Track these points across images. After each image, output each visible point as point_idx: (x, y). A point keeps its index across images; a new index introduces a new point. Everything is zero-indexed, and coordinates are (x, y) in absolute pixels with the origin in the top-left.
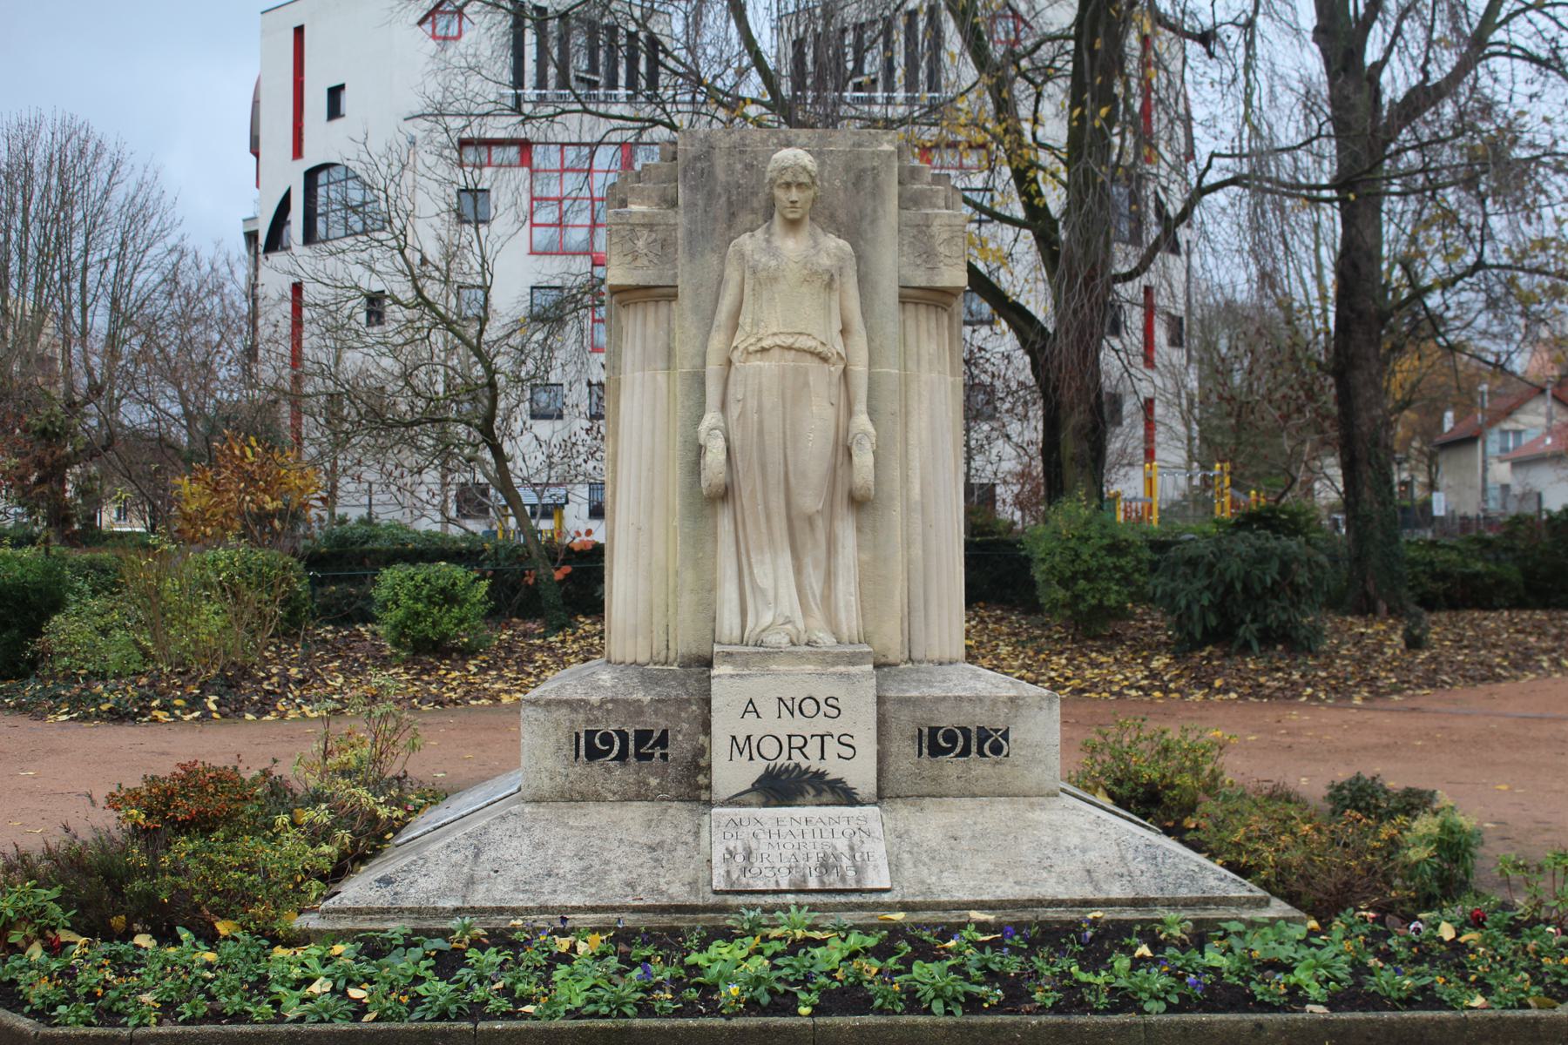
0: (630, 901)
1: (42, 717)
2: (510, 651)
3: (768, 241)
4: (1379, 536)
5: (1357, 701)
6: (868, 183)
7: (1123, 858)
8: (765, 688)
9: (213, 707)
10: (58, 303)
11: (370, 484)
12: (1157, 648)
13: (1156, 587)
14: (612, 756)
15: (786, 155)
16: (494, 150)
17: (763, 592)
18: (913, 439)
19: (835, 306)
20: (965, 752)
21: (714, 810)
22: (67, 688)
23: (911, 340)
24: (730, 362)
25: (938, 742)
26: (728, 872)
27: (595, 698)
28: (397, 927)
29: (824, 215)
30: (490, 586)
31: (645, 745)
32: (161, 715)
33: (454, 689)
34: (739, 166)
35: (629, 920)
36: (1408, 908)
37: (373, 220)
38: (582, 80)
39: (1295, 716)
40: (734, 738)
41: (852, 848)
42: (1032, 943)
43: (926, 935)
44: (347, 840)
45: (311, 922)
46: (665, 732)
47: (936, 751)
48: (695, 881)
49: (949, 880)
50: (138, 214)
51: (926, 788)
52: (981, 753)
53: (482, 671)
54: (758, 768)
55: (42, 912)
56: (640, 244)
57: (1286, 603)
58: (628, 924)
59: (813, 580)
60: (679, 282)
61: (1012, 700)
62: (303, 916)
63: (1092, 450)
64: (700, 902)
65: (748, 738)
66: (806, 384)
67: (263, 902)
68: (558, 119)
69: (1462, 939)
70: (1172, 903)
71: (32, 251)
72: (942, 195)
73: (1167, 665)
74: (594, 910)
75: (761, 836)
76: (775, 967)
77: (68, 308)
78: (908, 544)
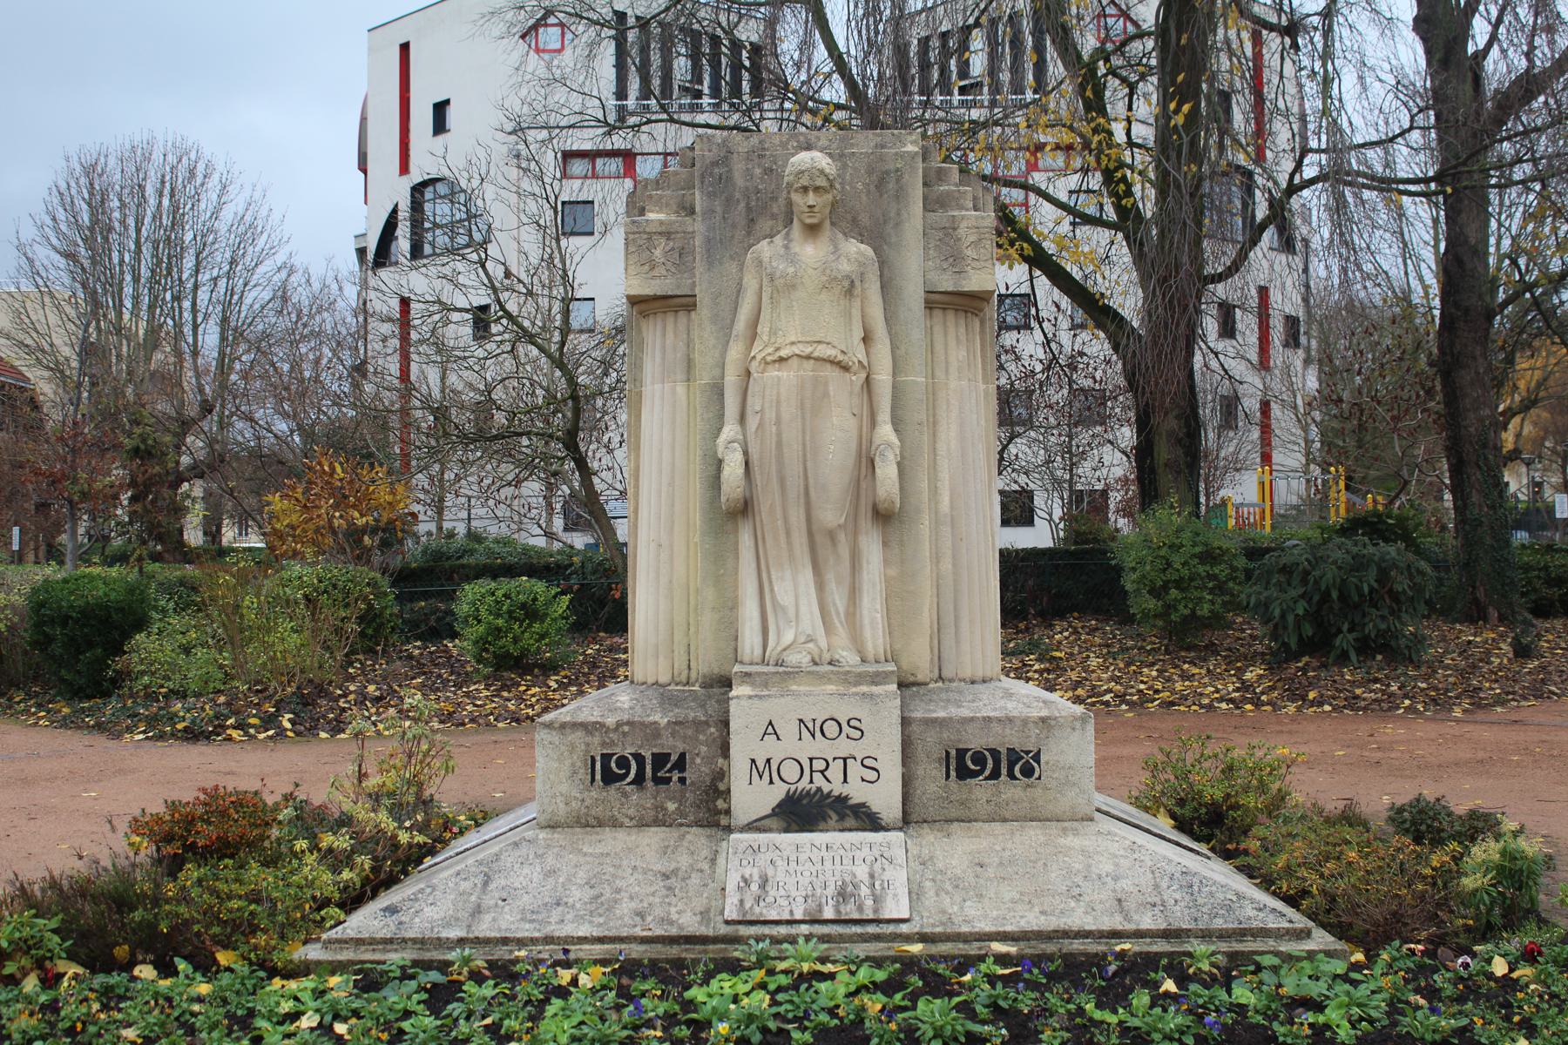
0: (638, 932)
1: (118, 736)
2: (594, 666)
3: (786, 247)
4: (1488, 541)
5: (1457, 713)
6: (891, 185)
7: (1156, 886)
8: (786, 708)
9: (288, 726)
10: (170, 322)
11: (470, 498)
12: (1251, 659)
13: (1249, 596)
14: (629, 780)
15: (803, 159)
16: (599, 162)
17: (783, 609)
18: (942, 448)
19: (856, 313)
20: (995, 775)
21: (733, 836)
22: (146, 707)
23: (939, 347)
24: (749, 373)
25: (967, 765)
26: (742, 902)
27: (610, 721)
28: (396, 958)
29: (842, 216)
30: (571, 601)
31: (662, 769)
32: (235, 734)
33: (532, 706)
34: (758, 171)
35: (636, 951)
36: (1463, 940)
37: (471, 237)
38: (687, 90)
39: (1391, 730)
40: (753, 761)
41: (872, 876)
42: (1053, 977)
43: (941, 969)
44: (367, 866)
45: (314, 953)
46: (682, 756)
47: (964, 774)
48: (708, 911)
49: (972, 909)
50: (248, 232)
51: (954, 813)
52: (1012, 776)
53: (563, 686)
54: (778, 792)
55: (39, 944)
56: (658, 252)
57: (1386, 612)
58: (634, 955)
59: (837, 597)
60: (697, 292)
61: (1043, 720)
62: (309, 946)
63: (1186, 454)
64: (711, 933)
65: (768, 761)
66: (826, 395)
67: (265, 931)
68: (644, 128)
69: (1515, 975)
70: (1206, 935)
71: (145, 273)
72: (970, 196)
73: (1261, 676)
74: (601, 940)
75: (779, 863)
76: (774, 1003)
77: (178, 326)
78: (937, 558)
